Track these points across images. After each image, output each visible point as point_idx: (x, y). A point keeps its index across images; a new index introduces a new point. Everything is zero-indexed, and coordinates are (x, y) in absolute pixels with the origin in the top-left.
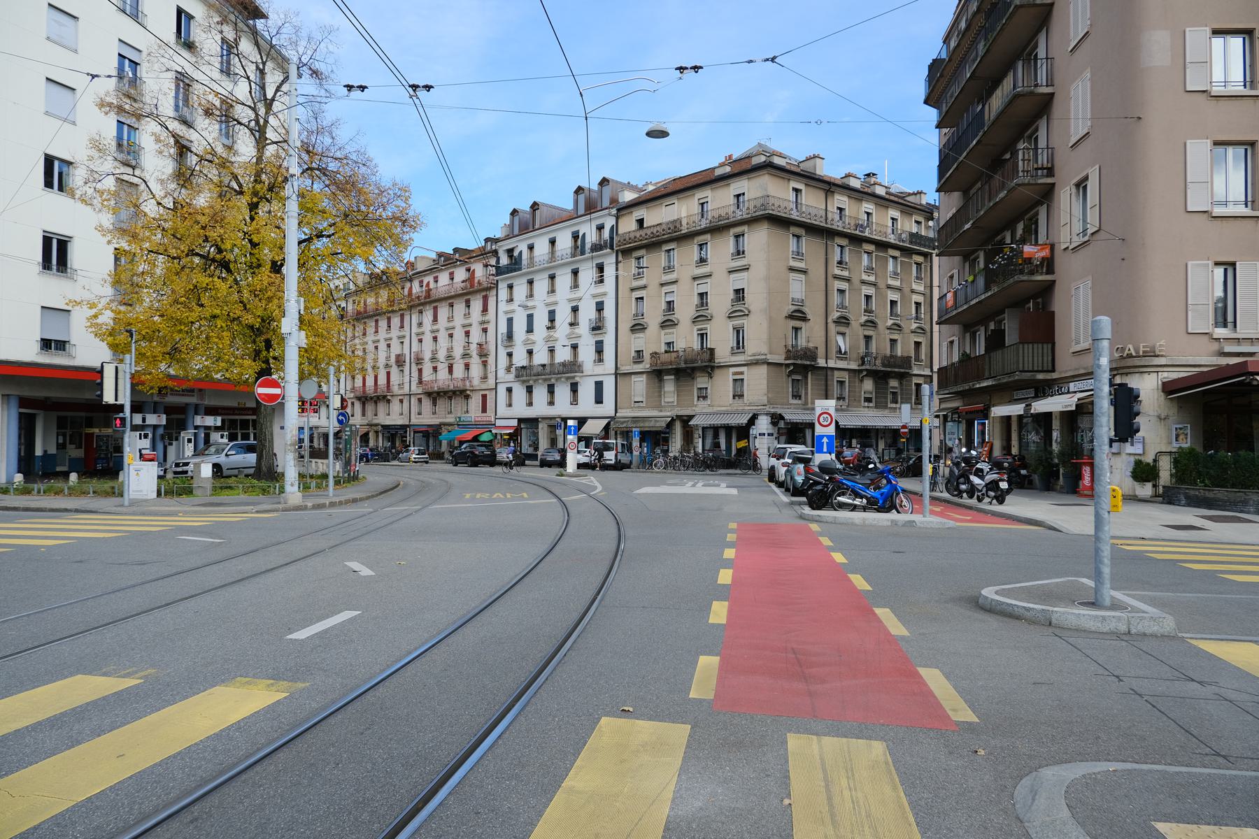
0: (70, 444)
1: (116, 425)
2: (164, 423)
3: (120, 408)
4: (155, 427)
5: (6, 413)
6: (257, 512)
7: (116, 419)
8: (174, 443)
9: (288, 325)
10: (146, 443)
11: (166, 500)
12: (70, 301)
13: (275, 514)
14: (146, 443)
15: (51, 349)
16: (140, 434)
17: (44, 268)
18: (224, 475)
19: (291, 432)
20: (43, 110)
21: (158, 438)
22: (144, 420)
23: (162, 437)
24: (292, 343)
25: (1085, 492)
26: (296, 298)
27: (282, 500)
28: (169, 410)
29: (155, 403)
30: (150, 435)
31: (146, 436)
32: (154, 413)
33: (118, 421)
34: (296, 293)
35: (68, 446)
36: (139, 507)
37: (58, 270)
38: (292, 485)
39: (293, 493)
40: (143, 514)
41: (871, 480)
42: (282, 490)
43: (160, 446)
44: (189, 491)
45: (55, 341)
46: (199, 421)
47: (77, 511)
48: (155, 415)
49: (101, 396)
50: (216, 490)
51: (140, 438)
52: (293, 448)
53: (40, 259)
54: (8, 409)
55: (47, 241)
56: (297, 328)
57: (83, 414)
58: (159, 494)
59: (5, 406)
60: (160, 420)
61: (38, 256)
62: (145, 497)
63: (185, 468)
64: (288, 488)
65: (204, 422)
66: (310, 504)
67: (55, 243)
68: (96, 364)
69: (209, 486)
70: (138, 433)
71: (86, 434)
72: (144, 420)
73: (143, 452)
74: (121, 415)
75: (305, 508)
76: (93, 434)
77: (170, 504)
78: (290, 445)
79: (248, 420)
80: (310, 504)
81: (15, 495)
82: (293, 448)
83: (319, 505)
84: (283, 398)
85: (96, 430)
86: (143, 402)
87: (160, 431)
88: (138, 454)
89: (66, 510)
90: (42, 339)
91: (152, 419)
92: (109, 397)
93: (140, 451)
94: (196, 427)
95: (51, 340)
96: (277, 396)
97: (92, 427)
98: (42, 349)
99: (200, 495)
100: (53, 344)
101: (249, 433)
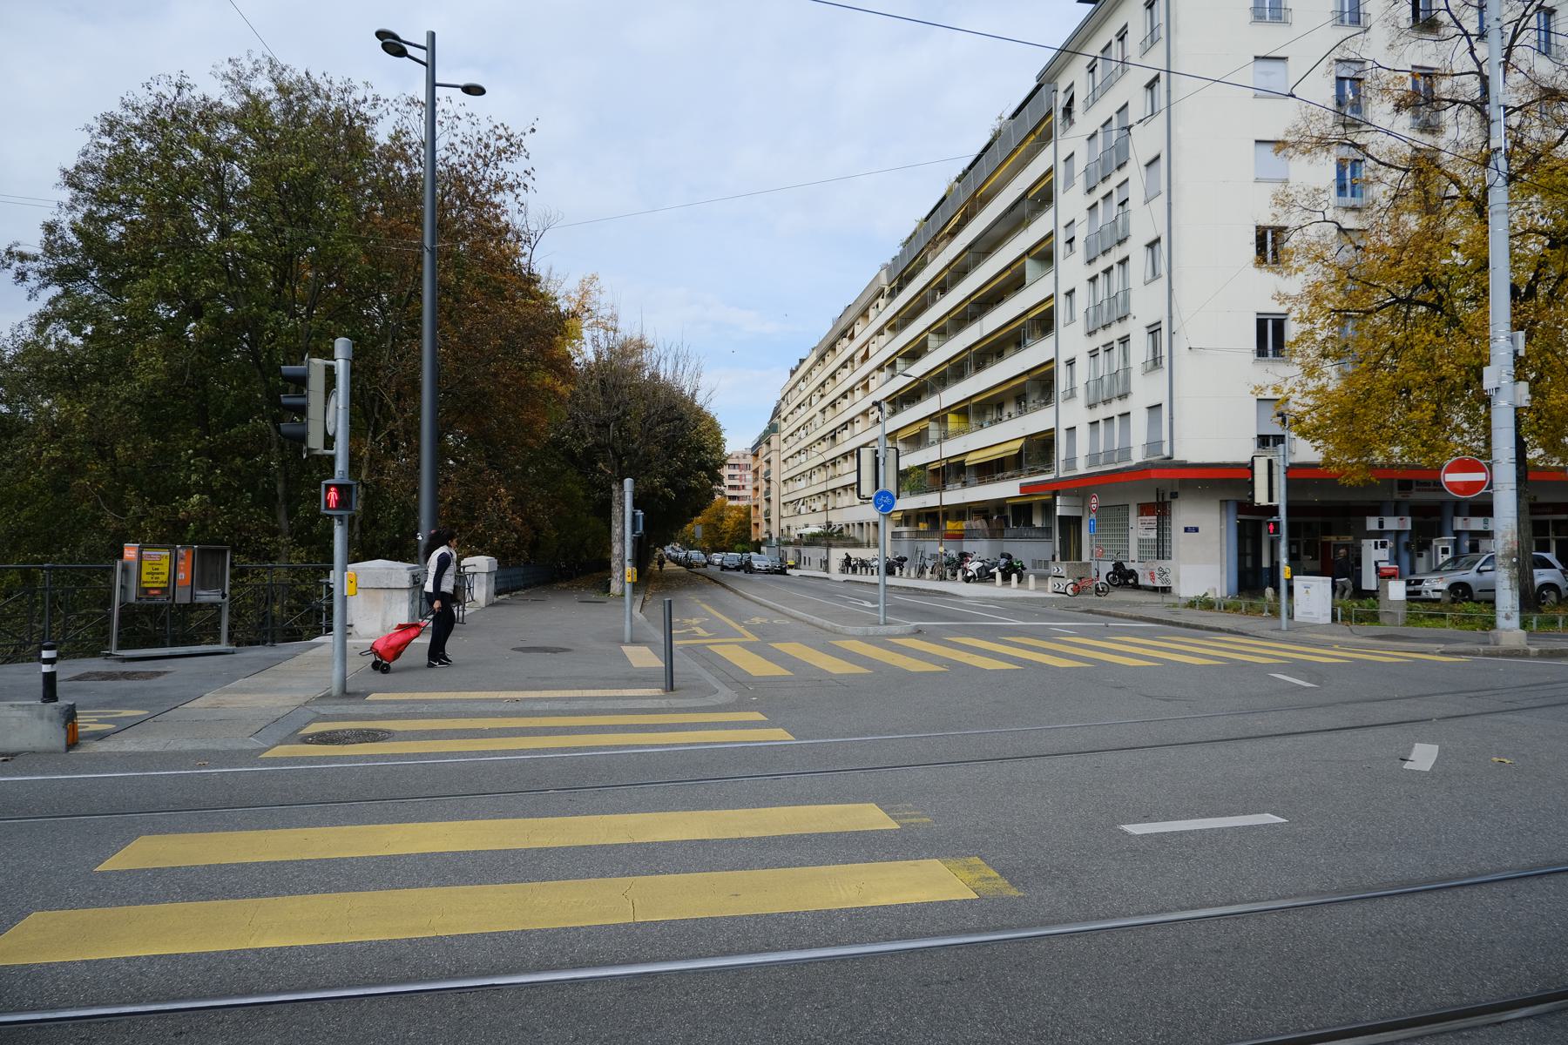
0: (1305, 554)
1: (327, 502)
2: (1409, 527)
3: (1274, 510)
4: (1398, 533)
5: (1225, 521)
6: (1443, 653)
7: (1268, 523)
8: (1425, 554)
9: (1497, 374)
10: (1383, 554)
11: (1341, 627)
12: (1256, 388)
13: (1464, 659)
14: (1383, 554)
15: (1268, 445)
16: (1376, 543)
17: (1259, 355)
18: (1475, 599)
19: (1503, 536)
20: (1253, 178)
21: (1402, 547)
22: (1381, 524)
23: (1407, 546)
24: (1503, 403)
25: (156, 592)
26: (1509, 334)
27: (1491, 640)
28: (1415, 511)
29: (1397, 502)
30: (1390, 544)
31: (1383, 545)
32: (1396, 515)
33: (1271, 527)
34: (1508, 327)
35: (1303, 557)
36: (1302, 634)
37: (1274, 355)
38: (1508, 618)
39: (1508, 630)
40: (1301, 643)
41: (785, 574)
42: (1491, 623)
43: (1405, 558)
44: (1374, 618)
45: (1274, 436)
46: (1459, 524)
47: (1230, 632)
48: (1397, 518)
49: (1253, 496)
50: (1413, 618)
51: (1376, 548)
52: (1507, 562)
53: (1254, 345)
54: (1227, 517)
55: (1261, 324)
56: (1512, 379)
57: (1319, 519)
58: (1334, 618)
59: (1224, 512)
60: (1404, 525)
61: (1105, 343)
62: (1317, 622)
63: (1418, 587)
64: (1501, 622)
65: (1467, 525)
66: (1533, 649)
67: (1270, 324)
68: (1246, 459)
69: (1401, 612)
70: (1373, 541)
71: (1323, 543)
72: (1381, 524)
73: (1381, 565)
74: (1275, 518)
75: (1525, 654)
76: (1329, 543)
77: (1343, 633)
78: (1503, 557)
79: (1547, 521)
80: (1533, 649)
81: (1201, 609)
82: (1507, 562)
83: (1551, 652)
84: (1490, 486)
85: (1333, 539)
86: (1381, 502)
87: (1405, 539)
88: (1374, 568)
89: (1220, 630)
90: (1259, 436)
91: (1392, 523)
92: (1261, 498)
93: (1376, 563)
94: (1457, 533)
95: (1268, 436)
96: (1480, 484)
97: (1330, 535)
98: (1259, 447)
99: (1387, 622)
100: (1271, 441)
101: (1548, 541)
